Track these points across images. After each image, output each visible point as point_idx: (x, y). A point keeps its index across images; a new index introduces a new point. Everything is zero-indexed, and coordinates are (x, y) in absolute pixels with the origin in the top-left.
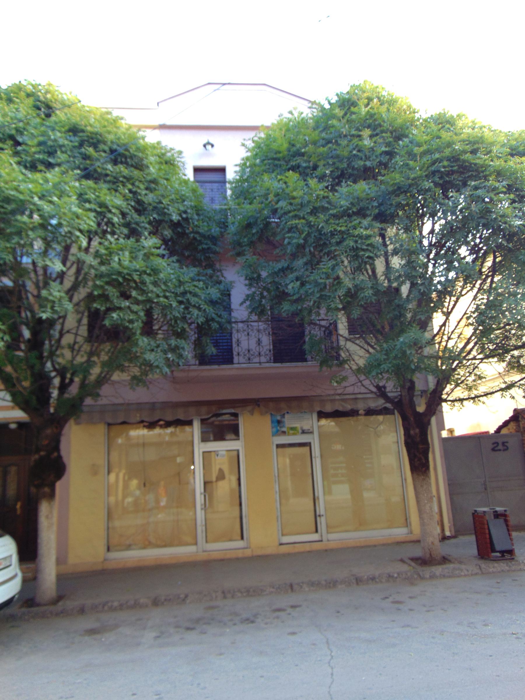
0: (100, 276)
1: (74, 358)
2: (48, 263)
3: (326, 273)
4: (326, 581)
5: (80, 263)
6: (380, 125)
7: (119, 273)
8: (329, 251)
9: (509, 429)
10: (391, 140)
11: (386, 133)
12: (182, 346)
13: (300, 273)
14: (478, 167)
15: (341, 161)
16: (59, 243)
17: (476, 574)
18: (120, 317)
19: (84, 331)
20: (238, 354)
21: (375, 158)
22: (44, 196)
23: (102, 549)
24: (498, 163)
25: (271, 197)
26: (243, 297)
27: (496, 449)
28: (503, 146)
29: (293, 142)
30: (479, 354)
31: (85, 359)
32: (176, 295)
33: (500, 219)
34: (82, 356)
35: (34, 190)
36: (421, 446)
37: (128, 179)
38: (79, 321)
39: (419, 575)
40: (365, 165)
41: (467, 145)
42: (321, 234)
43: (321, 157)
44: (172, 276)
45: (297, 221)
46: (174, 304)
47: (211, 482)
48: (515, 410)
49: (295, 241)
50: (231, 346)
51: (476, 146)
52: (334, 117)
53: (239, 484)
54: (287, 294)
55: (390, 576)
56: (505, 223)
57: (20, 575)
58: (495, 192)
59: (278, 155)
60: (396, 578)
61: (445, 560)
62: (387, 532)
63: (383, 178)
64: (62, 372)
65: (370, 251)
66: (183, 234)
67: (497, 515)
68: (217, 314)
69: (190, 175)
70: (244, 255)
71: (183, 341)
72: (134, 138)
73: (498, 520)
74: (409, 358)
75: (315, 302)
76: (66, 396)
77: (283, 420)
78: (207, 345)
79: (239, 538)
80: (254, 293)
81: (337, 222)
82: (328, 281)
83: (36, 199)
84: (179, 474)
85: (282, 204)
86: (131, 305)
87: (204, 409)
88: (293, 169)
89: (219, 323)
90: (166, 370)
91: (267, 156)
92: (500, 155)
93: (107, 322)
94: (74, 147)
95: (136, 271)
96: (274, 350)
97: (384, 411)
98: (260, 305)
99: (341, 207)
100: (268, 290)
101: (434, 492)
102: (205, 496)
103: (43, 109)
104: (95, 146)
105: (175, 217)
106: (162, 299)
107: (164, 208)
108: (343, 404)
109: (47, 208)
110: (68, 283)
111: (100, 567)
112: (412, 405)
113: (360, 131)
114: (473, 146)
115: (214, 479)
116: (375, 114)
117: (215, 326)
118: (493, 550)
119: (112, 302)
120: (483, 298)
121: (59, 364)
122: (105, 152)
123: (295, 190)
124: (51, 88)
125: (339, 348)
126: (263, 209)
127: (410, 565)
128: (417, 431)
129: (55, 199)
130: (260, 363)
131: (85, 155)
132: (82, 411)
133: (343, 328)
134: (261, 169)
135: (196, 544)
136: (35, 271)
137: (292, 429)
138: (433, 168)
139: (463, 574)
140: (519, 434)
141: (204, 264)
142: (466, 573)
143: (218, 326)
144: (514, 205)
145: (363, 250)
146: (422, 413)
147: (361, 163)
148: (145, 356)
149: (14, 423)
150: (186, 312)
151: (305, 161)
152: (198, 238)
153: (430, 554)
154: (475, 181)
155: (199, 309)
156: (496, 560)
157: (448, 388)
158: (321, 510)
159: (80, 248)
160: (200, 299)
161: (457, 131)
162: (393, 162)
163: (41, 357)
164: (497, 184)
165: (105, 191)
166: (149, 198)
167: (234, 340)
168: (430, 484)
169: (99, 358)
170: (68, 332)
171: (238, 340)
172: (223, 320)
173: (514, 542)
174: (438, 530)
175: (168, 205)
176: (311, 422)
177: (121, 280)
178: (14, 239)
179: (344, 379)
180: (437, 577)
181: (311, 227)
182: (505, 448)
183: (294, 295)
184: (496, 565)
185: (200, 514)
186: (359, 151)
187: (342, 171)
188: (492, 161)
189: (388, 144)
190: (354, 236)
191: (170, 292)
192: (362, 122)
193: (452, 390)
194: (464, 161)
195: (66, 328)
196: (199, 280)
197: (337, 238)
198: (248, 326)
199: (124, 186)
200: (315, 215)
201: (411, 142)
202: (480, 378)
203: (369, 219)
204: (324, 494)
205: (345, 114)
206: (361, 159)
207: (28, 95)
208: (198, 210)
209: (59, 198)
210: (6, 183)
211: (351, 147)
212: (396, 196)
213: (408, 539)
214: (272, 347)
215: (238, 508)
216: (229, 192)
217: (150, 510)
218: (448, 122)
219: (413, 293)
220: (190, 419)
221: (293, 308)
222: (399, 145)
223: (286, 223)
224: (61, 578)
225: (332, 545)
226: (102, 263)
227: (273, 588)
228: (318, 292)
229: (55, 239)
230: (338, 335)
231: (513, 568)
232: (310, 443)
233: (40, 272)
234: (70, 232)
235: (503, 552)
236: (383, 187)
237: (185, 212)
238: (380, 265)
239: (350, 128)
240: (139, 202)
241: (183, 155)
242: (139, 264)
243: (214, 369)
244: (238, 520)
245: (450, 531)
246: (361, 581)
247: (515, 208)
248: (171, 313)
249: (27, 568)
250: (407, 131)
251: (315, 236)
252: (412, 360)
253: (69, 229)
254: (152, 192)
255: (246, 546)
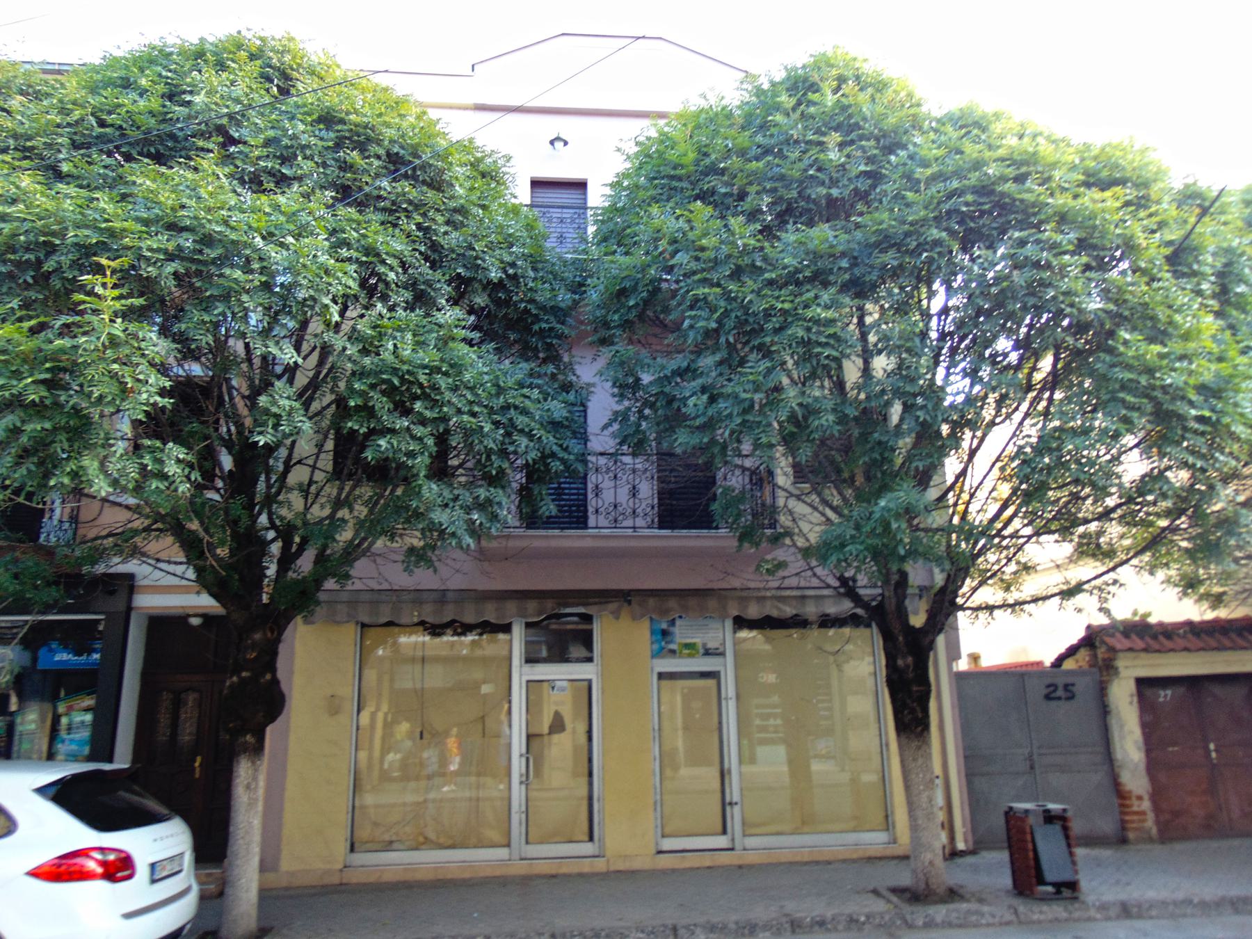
0: (360, 374)
1: (307, 509)
2: (273, 350)
3: (754, 382)
4: (737, 923)
5: (326, 350)
6: (857, 126)
7: (395, 371)
8: (760, 344)
9: (1077, 661)
10: (875, 152)
11: (868, 140)
12: (497, 499)
13: (710, 381)
14: (1027, 207)
15: (787, 187)
16: (294, 317)
17: (1008, 923)
18: (393, 447)
19: (326, 462)
20: (597, 511)
21: (846, 182)
22: (271, 234)
23: (342, 847)
24: (1061, 201)
25: (663, 245)
26: (608, 415)
27: (1053, 695)
28: (1073, 168)
29: (705, 150)
30: (1025, 526)
31: (327, 512)
32: (491, 411)
33: (1061, 298)
34: (322, 507)
35: (255, 225)
36: (915, 688)
37: (417, 206)
38: (320, 446)
39: (906, 922)
40: (829, 196)
41: (1009, 166)
42: (747, 314)
43: (754, 178)
44: (486, 378)
45: (707, 290)
46: (487, 427)
47: (540, 735)
48: (1089, 627)
49: (701, 324)
50: (585, 495)
51: (1024, 169)
52: (777, 108)
53: (590, 739)
54: (686, 417)
55: (852, 921)
56: (1072, 305)
57: (195, 889)
58: (1054, 251)
59: (678, 172)
60: (864, 923)
61: (953, 894)
62: (852, 838)
63: (859, 219)
64: (285, 533)
65: (833, 347)
66: (507, 302)
67: (1049, 818)
68: (561, 446)
69: (523, 194)
70: (612, 344)
71: (501, 492)
72: (429, 132)
73: (1049, 827)
74: (895, 535)
75: (732, 433)
76: (291, 575)
77: (671, 629)
78: (542, 500)
79: (586, 838)
80: (629, 409)
81: (776, 293)
82: (757, 397)
83: (259, 241)
84: (483, 718)
85: (682, 258)
86: (412, 426)
87: (532, 605)
88: (703, 196)
89: (563, 461)
90: (468, 540)
91: (659, 172)
92: (1066, 185)
93: (369, 455)
94: (328, 148)
95: (425, 367)
96: (660, 505)
97: (853, 620)
98: (638, 431)
99: (784, 268)
100: (652, 406)
101: (938, 770)
102: (528, 760)
103: (276, 81)
104: (362, 147)
105: (495, 275)
106: (465, 418)
107: (477, 258)
108: (780, 605)
109: (276, 255)
110: (301, 380)
111: (335, 880)
112: (902, 614)
113: (824, 134)
114: (1018, 168)
115: (546, 730)
116: (850, 106)
117: (556, 466)
118: (1041, 881)
119: (379, 420)
120: (1032, 431)
121: (282, 518)
122: (378, 157)
123: (705, 235)
124: (292, 46)
125: (774, 509)
126: (649, 266)
127: (889, 901)
128: (910, 660)
129: (290, 240)
130: (634, 528)
131: (345, 162)
132: (318, 603)
133: (783, 478)
134: (649, 194)
135: (508, 845)
136: (249, 360)
137: (687, 646)
138: (945, 207)
139: (984, 921)
140: (1094, 670)
141: (541, 355)
142: (991, 920)
143: (561, 467)
144: (1087, 274)
145: (820, 344)
146: (920, 629)
147: (823, 191)
148: (432, 516)
149: (196, 615)
150: (507, 441)
151: (726, 184)
152: (534, 311)
153: (927, 884)
154: (1021, 230)
155: (530, 436)
156: (1044, 899)
157: (969, 584)
158: (734, 794)
159: (327, 324)
160: (533, 419)
161: (991, 141)
162: (878, 190)
163: (250, 506)
164: (1059, 238)
165: (375, 226)
166: (452, 239)
167: (590, 486)
168: (928, 757)
169: (351, 510)
170: (299, 462)
171: (597, 487)
172: (572, 457)
173: (1079, 867)
174: (944, 837)
175: (484, 252)
176: (721, 635)
177: (396, 382)
178: (216, 308)
179: (782, 565)
180: (937, 925)
181: (730, 299)
182: (1069, 694)
183: (697, 416)
184: (1045, 908)
185: (518, 792)
186: (819, 170)
187: (789, 204)
188: (1052, 195)
189: (870, 160)
190: (805, 320)
191: (480, 404)
192: (827, 119)
193: (975, 590)
194: (1003, 195)
195: (296, 456)
196: (531, 386)
197: (775, 322)
198: (615, 462)
199: (407, 217)
200: (739, 280)
201: (911, 157)
202: (1027, 568)
203: (833, 290)
204: (741, 762)
205: (799, 103)
206: (823, 184)
207: (252, 57)
208: (535, 261)
209: (298, 237)
210: (209, 210)
211: (806, 162)
212: (880, 252)
213: (889, 852)
214: (656, 501)
215: (585, 780)
216: (591, 229)
217: (429, 777)
218: (977, 124)
219: (907, 421)
220: (507, 621)
221: (695, 440)
222: (889, 162)
223: (688, 292)
224: (265, 895)
225: (751, 858)
226: (365, 352)
227: (643, 932)
228: (738, 414)
229: (285, 309)
230: (775, 486)
231: (1077, 915)
232: (719, 672)
233: (257, 362)
234: (312, 298)
235: (1059, 886)
236: (858, 235)
237: (513, 265)
238: (852, 372)
239: (805, 128)
240: (435, 246)
241: (512, 162)
242: (429, 356)
243: (554, 537)
244: (585, 803)
245: (966, 841)
246: (799, 927)
247: (1089, 279)
248: (481, 442)
249: (209, 875)
250: (905, 138)
251: (737, 317)
252: (901, 540)
253: (312, 292)
254: (456, 229)
255: (597, 853)
